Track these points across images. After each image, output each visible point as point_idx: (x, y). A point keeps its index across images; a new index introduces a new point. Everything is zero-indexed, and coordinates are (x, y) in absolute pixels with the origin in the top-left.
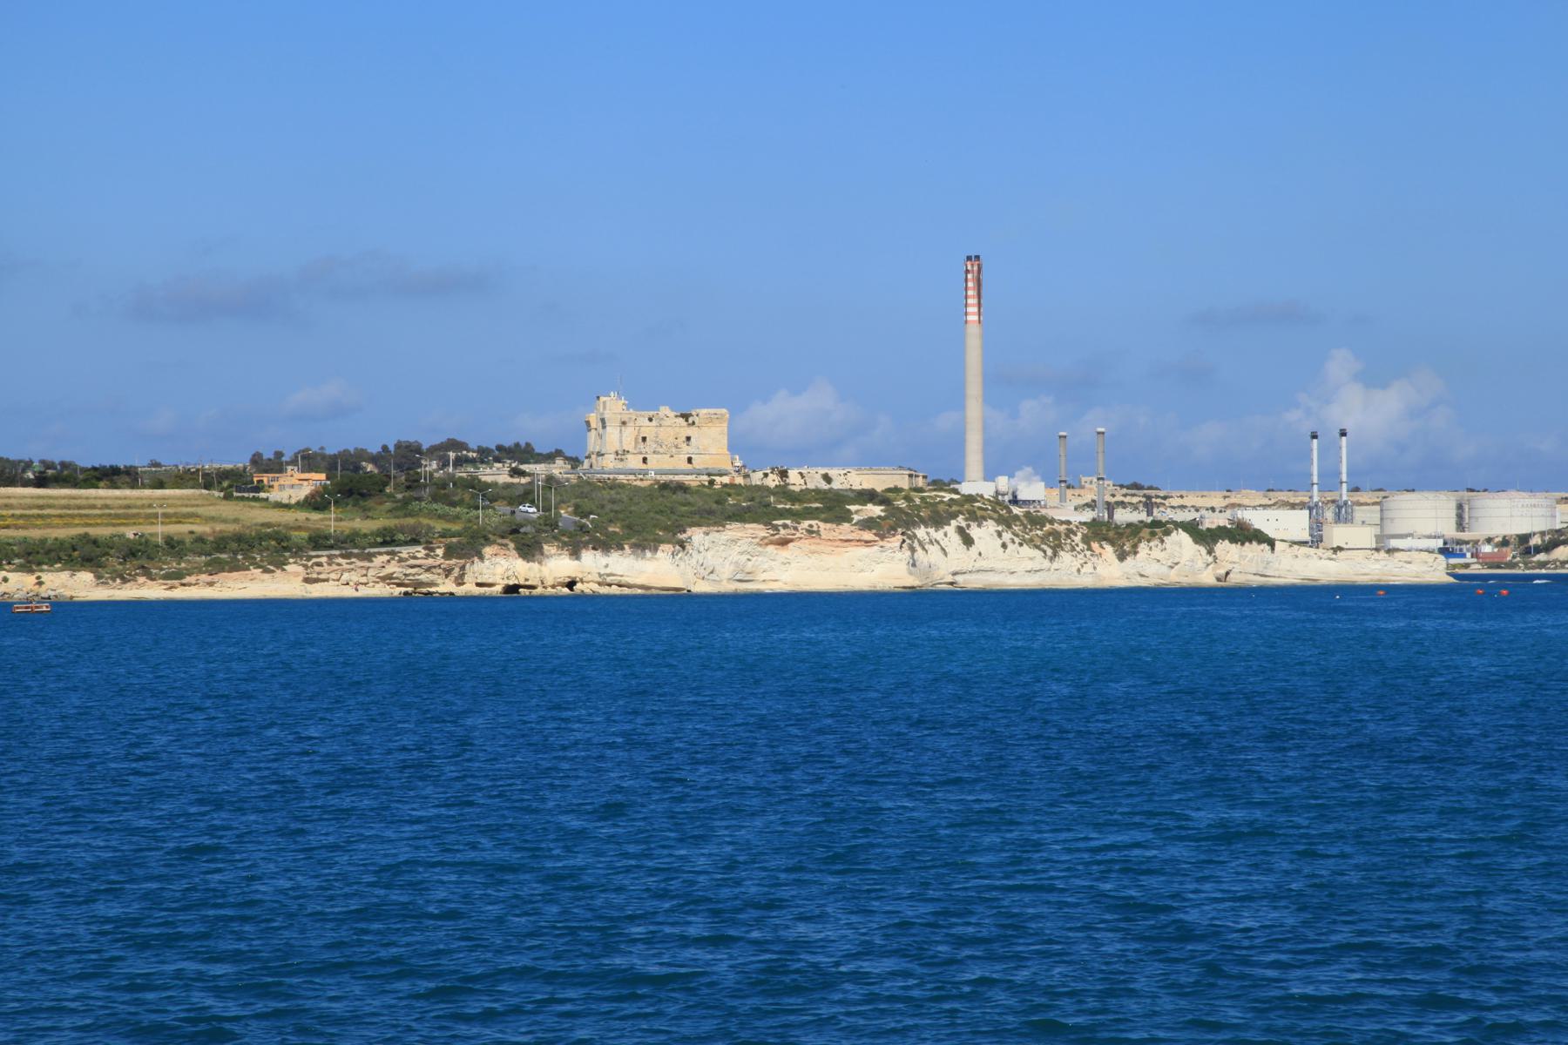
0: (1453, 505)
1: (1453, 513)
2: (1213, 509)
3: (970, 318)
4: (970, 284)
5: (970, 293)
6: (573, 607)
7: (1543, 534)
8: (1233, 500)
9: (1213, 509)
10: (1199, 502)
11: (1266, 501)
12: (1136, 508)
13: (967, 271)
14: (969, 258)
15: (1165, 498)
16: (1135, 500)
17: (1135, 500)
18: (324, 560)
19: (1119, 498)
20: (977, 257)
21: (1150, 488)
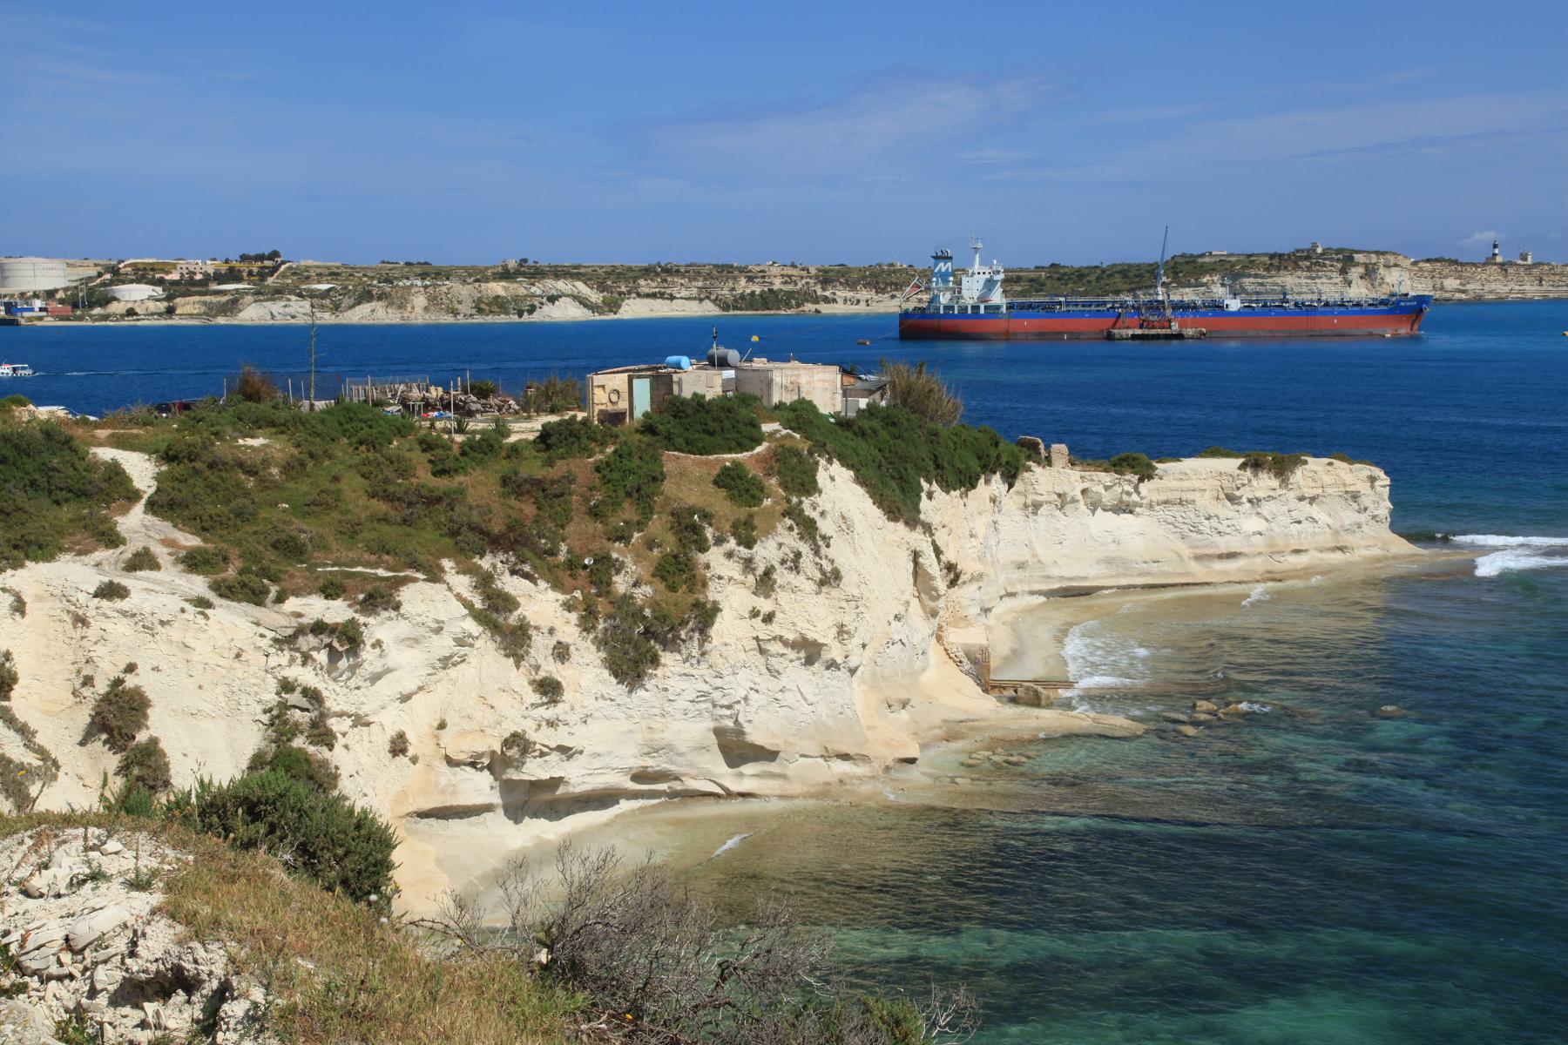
7: (66, 289)
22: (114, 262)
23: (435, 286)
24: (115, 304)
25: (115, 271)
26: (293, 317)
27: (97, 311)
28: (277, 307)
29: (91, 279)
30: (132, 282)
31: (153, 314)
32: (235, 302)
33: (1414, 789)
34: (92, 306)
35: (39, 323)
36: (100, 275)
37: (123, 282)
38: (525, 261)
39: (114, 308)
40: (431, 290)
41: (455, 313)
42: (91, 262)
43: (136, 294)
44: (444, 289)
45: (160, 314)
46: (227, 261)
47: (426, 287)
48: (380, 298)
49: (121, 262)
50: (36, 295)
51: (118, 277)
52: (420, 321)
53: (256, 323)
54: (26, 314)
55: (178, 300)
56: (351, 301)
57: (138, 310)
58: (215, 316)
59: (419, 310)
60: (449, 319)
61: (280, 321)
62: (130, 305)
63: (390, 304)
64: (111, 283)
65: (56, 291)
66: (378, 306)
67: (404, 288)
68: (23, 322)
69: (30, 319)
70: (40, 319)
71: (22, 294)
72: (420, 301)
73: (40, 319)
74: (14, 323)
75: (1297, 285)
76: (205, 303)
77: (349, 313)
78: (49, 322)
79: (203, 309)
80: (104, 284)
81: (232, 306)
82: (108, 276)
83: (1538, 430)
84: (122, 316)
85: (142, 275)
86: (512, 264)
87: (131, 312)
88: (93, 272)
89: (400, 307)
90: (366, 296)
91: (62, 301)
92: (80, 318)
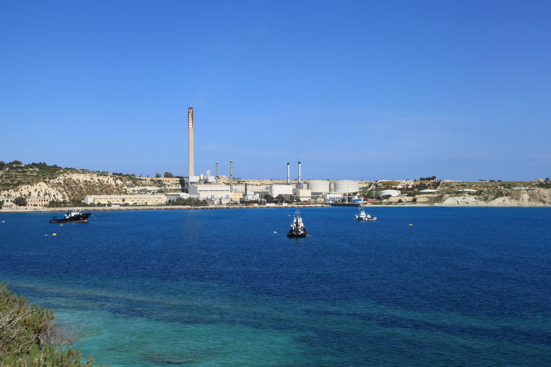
4: (190, 116)
6: (175, 209)
7: (360, 192)
8: (262, 182)
10: (253, 183)
13: (189, 112)
16: (235, 182)
17: (235, 182)
18: (224, 202)
20: (192, 108)
23: (532, 190)
26: (467, 203)
28: (460, 199)
29: (367, 188)
30: (384, 189)
31: (408, 202)
32: (441, 197)
38: (548, 179)
39: (391, 199)
40: (530, 191)
41: (545, 203)
42: (364, 182)
44: (536, 191)
45: (411, 202)
46: (415, 181)
47: (527, 190)
48: (507, 195)
49: (377, 181)
52: (527, 205)
53: (451, 205)
55: (417, 196)
56: (493, 196)
58: (434, 203)
59: (526, 200)
60: (541, 205)
61: (461, 205)
63: (512, 198)
65: (357, 193)
66: (506, 198)
67: (517, 190)
72: (526, 196)
73: (366, 204)
75: (75, 177)
76: (428, 197)
77: (493, 201)
79: (428, 200)
81: (440, 199)
83: (417, 326)
86: (542, 180)
88: (367, 185)
89: (517, 199)
90: (500, 194)
92: (381, 204)
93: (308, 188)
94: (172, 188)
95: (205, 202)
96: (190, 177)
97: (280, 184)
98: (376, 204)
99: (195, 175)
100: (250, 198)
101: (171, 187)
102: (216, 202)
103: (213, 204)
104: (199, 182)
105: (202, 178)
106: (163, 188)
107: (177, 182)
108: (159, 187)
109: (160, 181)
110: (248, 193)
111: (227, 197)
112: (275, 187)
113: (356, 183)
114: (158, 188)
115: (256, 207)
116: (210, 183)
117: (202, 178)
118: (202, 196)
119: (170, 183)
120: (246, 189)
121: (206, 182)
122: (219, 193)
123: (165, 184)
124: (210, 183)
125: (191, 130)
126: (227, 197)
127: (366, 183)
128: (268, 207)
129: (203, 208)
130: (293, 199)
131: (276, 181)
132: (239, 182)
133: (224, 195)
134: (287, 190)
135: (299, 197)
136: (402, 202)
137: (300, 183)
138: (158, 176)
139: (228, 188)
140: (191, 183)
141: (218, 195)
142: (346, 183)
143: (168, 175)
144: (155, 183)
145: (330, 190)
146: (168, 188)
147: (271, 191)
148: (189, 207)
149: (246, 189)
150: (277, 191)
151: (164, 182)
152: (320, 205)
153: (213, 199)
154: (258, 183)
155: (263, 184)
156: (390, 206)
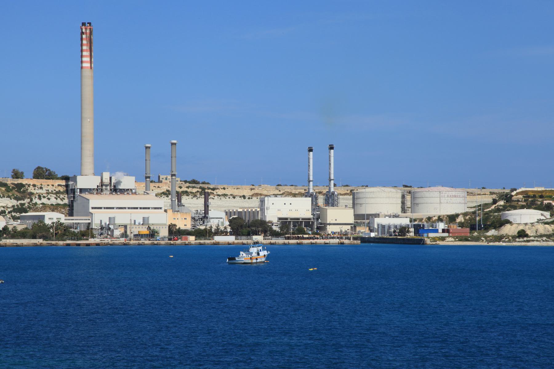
0: (400, 195)
1: (400, 201)
2: (244, 197)
3: (84, 65)
4: (85, 42)
5: (85, 48)
7: (465, 214)
8: (256, 191)
9: (244, 197)
10: (236, 192)
11: (277, 192)
12: (195, 196)
13: (82, 33)
14: (84, 24)
15: (214, 189)
16: (194, 190)
17: (194, 190)
19: (184, 189)
21: (203, 183)
22: (507, 191)
24: (508, 226)
25: (507, 198)
27: (492, 232)
29: (486, 205)
30: (522, 207)
31: (541, 236)
33: (143, 241)
34: (487, 229)
35: (441, 243)
36: (495, 202)
37: (515, 208)
39: (507, 230)
42: (487, 191)
43: (525, 218)
49: (513, 190)
50: (440, 219)
51: (510, 203)
54: (431, 235)
57: (528, 232)
62: (521, 228)
64: (505, 208)
65: (457, 215)
68: (428, 242)
69: (434, 239)
70: (443, 239)
71: (429, 219)
73: (443, 239)
74: (420, 242)
78: (450, 242)
80: (498, 210)
82: (502, 203)
84: (514, 237)
85: (532, 201)
87: (522, 234)
88: (489, 199)
91: (461, 225)
92: (477, 239)
93: (354, 205)
94: (49, 202)
95: (106, 229)
96: (79, 178)
97: (295, 195)
98: (467, 240)
99: (94, 174)
100: (213, 224)
101: (44, 201)
102: (117, 233)
103: (112, 236)
104: (99, 190)
105: (106, 180)
106: (27, 201)
107: (62, 189)
108: (17, 199)
109: (22, 185)
110: (211, 214)
111: (145, 221)
112: (269, 201)
113: (460, 192)
114: (14, 202)
115: (190, 244)
116: (123, 191)
117: (106, 180)
118: (99, 218)
119: (43, 191)
120: (206, 206)
121: (116, 190)
122: (133, 212)
123: (31, 194)
124: (123, 191)
125: (87, 73)
126: (145, 221)
127: (492, 193)
128: (217, 244)
129: (68, 245)
130: (288, 229)
131: (288, 189)
132: (203, 189)
133: (138, 216)
134: (301, 208)
135: (326, 224)
136: (527, 236)
137: (333, 194)
138: (17, 175)
139: (165, 202)
140: (81, 190)
141: (122, 218)
142: (437, 194)
143: (41, 173)
144: (8, 189)
145: (404, 210)
146: (39, 202)
147: (262, 210)
148: (41, 241)
149: (206, 206)
150: (282, 207)
151: (31, 189)
152: (336, 241)
153: (111, 227)
154: (247, 192)
155: (257, 195)
156: (497, 244)
